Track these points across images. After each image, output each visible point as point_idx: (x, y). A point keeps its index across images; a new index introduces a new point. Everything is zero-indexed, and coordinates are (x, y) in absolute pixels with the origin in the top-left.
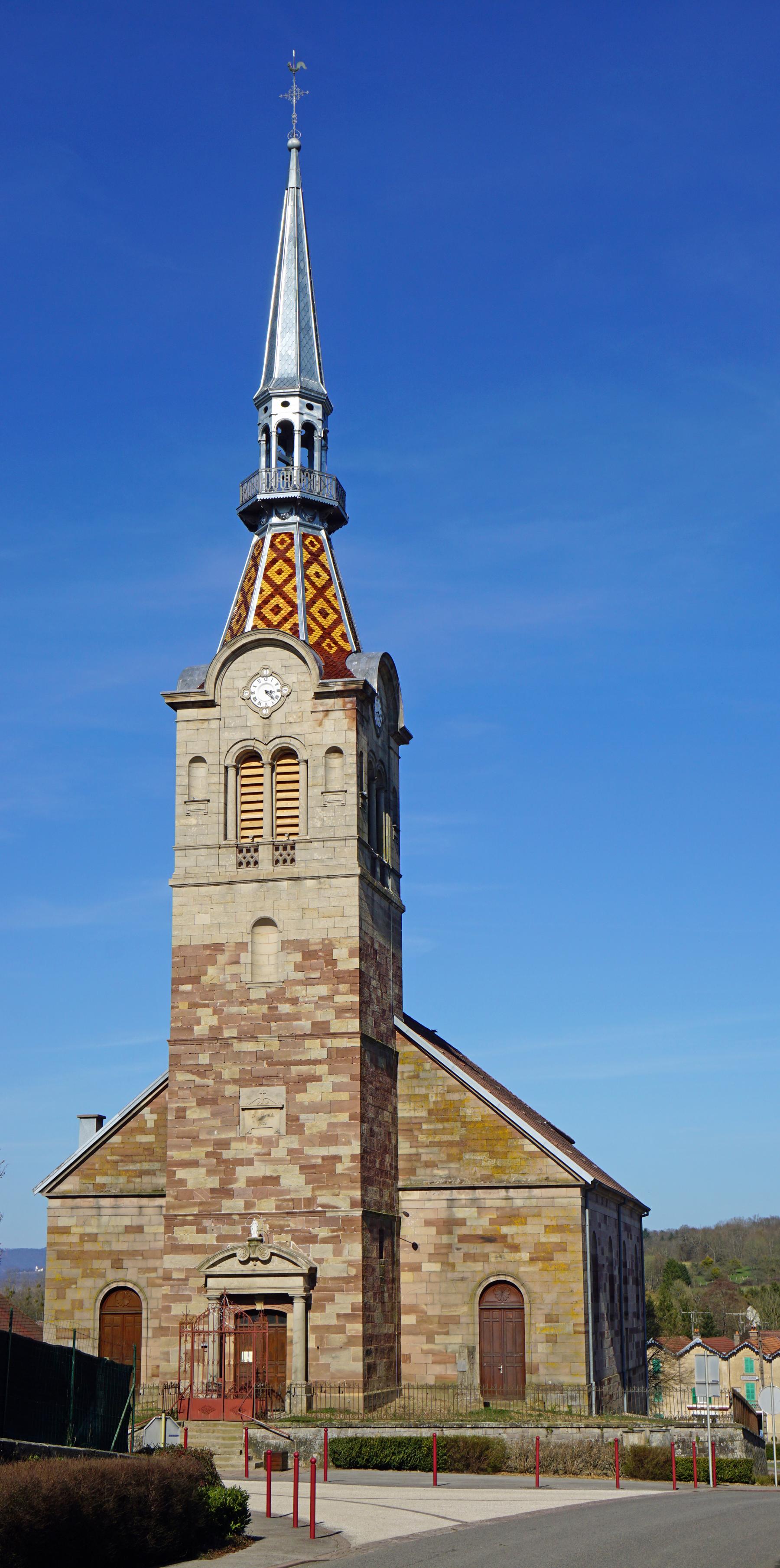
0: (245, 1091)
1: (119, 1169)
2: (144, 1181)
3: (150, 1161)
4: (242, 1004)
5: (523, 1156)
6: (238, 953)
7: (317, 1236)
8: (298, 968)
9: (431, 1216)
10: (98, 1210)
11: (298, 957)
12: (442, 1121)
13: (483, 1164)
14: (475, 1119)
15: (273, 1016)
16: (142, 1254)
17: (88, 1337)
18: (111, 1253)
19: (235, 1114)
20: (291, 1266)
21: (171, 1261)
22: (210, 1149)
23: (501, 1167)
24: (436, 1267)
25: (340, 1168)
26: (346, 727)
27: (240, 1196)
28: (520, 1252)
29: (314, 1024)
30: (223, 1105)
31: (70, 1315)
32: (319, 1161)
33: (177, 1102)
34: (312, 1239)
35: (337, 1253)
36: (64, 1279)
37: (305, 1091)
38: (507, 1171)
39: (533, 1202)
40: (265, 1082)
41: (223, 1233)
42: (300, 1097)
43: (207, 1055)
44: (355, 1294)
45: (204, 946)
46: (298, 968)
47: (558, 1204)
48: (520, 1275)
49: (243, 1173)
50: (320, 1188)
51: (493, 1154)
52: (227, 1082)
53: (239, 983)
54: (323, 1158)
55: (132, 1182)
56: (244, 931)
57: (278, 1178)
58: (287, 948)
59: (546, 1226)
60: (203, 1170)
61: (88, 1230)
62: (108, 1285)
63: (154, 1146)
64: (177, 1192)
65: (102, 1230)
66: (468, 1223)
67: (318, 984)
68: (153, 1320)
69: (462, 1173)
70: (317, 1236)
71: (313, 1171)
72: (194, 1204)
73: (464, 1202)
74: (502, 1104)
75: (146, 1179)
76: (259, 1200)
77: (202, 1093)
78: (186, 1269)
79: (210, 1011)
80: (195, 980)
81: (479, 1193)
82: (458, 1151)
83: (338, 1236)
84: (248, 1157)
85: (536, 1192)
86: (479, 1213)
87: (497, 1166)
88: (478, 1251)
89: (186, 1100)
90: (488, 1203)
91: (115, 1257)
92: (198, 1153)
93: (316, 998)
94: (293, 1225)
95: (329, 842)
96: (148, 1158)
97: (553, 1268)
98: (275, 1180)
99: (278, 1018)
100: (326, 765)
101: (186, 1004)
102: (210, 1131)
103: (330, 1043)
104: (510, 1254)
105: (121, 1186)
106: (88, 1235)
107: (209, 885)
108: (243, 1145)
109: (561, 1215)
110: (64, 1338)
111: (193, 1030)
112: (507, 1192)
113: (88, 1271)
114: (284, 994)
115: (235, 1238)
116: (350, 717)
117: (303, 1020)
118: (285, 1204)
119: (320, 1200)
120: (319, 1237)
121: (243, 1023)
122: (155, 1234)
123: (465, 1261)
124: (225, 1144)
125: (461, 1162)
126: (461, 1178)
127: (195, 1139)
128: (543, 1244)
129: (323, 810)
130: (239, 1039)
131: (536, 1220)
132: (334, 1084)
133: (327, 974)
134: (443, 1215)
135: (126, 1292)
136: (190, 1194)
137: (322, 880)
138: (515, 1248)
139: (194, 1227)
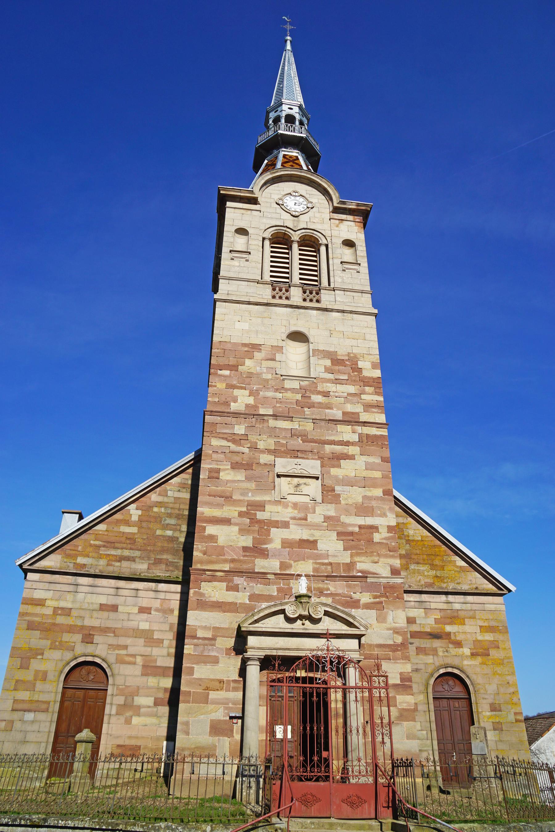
0: (279, 461)
1: (100, 552)
2: (123, 566)
3: (131, 549)
4: (277, 390)
5: (456, 569)
6: (273, 352)
7: (359, 601)
8: (327, 370)
10: (76, 586)
11: (328, 363)
13: (426, 573)
14: (416, 539)
16: (114, 631)
17: (47, 710)
18: (83, 627)
19: (270, 480)
20: (345, 627)
22: (244, 509)
23: (440, 577)
25: (377, 537)
26: (357, 231)
27: (274, 556)
28: (462, 647)
29: (344, 413)
30: (257, 471)
31: (30, 686)
32: (357, 529)
33: (210, 464)
35: (381, 619)
36: (31, 649)
37: (339, 466)
38: (445, 581)
39: (468, 606)
40: (300, 455)
41: (257, 593)
42: (334, 471)
43: (243, 427)
44: (403, 663)
45: (242, 344)
46: (327, 370)
47: (488, 609)
48: (465, 668)
50: (358, 554)
51: (433, 567)
52: (262, 452)
53: (274, 375)
54: (360, 527)
55: (111, 565)
56: (279, 338)
57: (315, 542)
58: (318, 355)
59: (481, 627)
60: (236, 528)
61: (63, 604)
62: (76, 658)
63: (136, 537)
64: (206, 547)
65: (77, 605)
66: (417, 622)
67: (346, 384)
68: (118, 697)
69: (409, 580)
70: (359, 601)
71: (351, 538)
72: (225, 561)
73: (413, 603)
74: (439, 527)
75: (125, 564)
76: (295, 561)
77: (237, 458)
78: (214, 628)
79: (247, 392)
80: (234, 368)
81: (425, 597)
82: (405, 562)
83: (381, 603)
84: (283, 519)
85: (470, 598)
86: (426, 614)
87: (437, 576)
88: (428, 646)
89: (219, 463)
90: (433, 606)
91: (86, 632)
92: (230, 512)
93: (346, 394)
94: (332, 589)
95: (349, 293)
96: (129, 546)
97: (490, 663)
98: (313, 544)
99: (311, 406)
101: (224, 385)
102: (244, 492)
103: (359, 429)
104: (455, 649)
105: (101, 568)
106: (62, 609)
107: (249, 303)
108: (279, 508)
109: (491, 618)
110: (20, 710)
111: (229, 405)
112: (447, 597)
113: (57, 643)
114: (317, 387)
116: (359, 226)
117: (335, 409)
118: (323, 567)
119: (360, 566)
120: (361, 602)
121: (278, 405)
122: (129, 613)
124: (261, 506)
125: (408, 571)
126: (409, 584)
127: (228, 498)
128: (480, 641)
129: (342, 273)
130: (275, 416)
131: (472, 622)
132: (367, 463)
133: (354, 378)
135: (92, 668)
136: (221, 551)
137: (345, 314)
138: (458, 644)
139: (224, 584)
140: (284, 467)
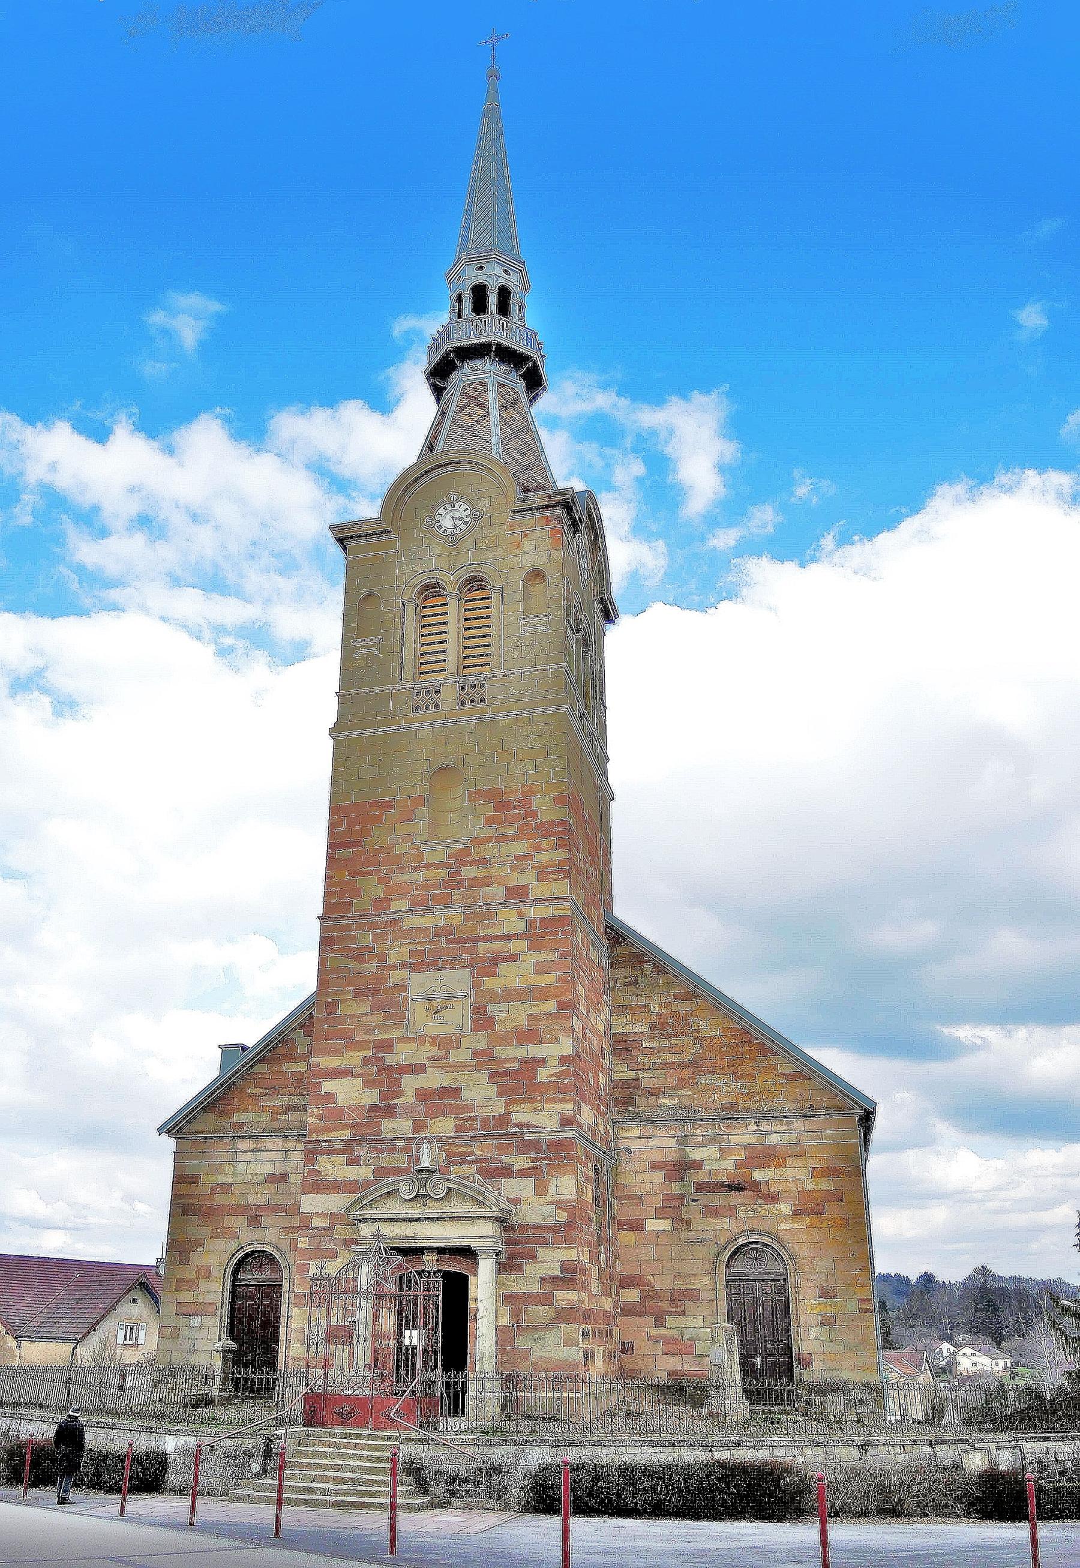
0: (417, 978)
9: (658, 1157)
11: (490, 810)
12: (669, 1036)
15: (455, 881)
21: (311, 1203)
22: (369, 1053)
24: (665, 1225)
25: (543, 1075)
32: (516, 1065)
34: (507, 1172)
35: (541, 1189)
42: (489, 983)
49: (410, 1084)
51: (737, 1077)
52: (394, 967)
65: (239, 1179)
72: (345, 1127)
90: (734, 1139)
91: (253, 1213)
92: (353, 1058)
98: (454, 1092)
99: (460, 884)
100: (526, 590)
115: (398, 1171)
119: (517, 1118)
123: (705, 1216)
124: (387, 1046)
132: (536, 964)
134: (673, 1156)
136: (340, 1113)
138: (773, 1199)
140: (421, 985)
